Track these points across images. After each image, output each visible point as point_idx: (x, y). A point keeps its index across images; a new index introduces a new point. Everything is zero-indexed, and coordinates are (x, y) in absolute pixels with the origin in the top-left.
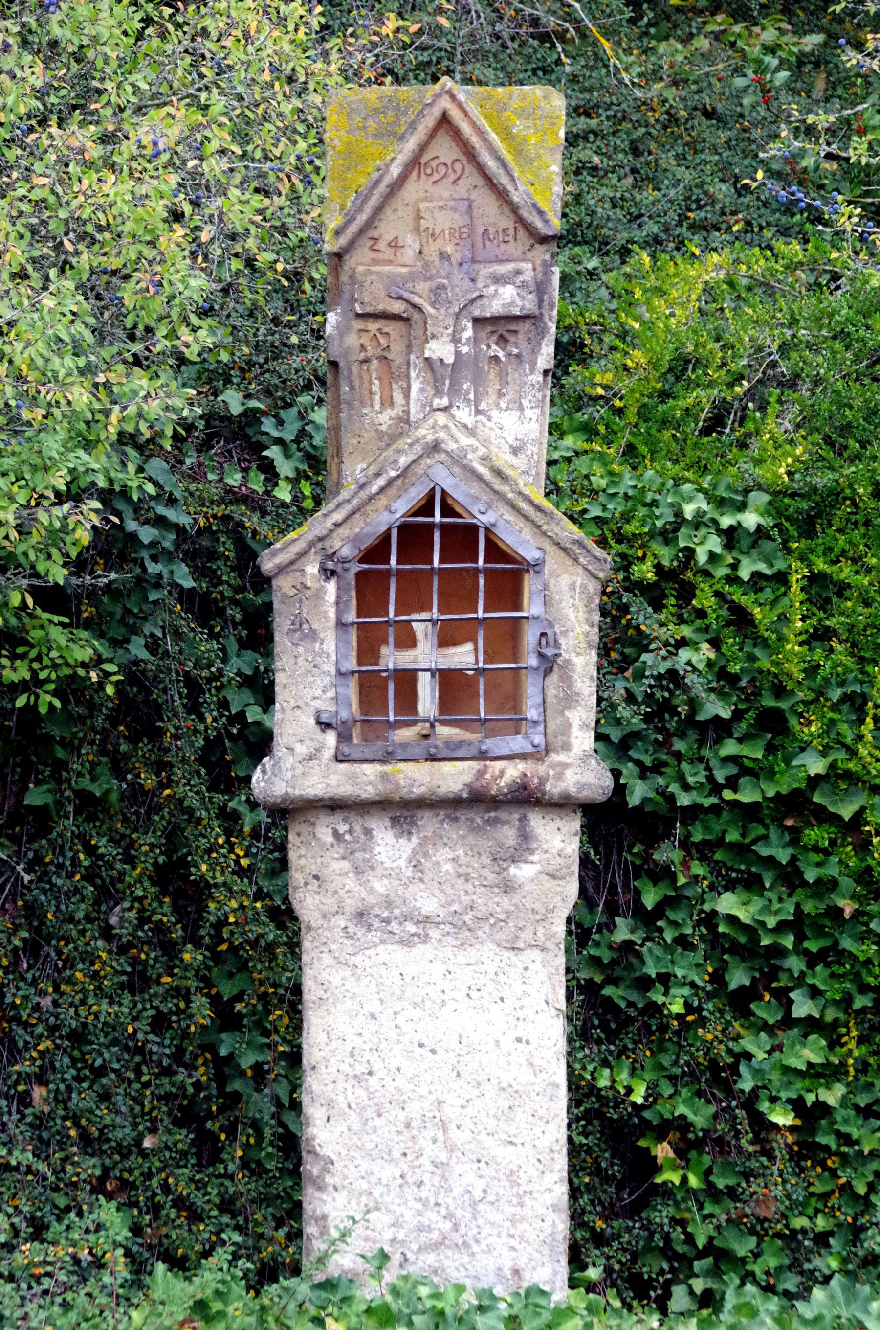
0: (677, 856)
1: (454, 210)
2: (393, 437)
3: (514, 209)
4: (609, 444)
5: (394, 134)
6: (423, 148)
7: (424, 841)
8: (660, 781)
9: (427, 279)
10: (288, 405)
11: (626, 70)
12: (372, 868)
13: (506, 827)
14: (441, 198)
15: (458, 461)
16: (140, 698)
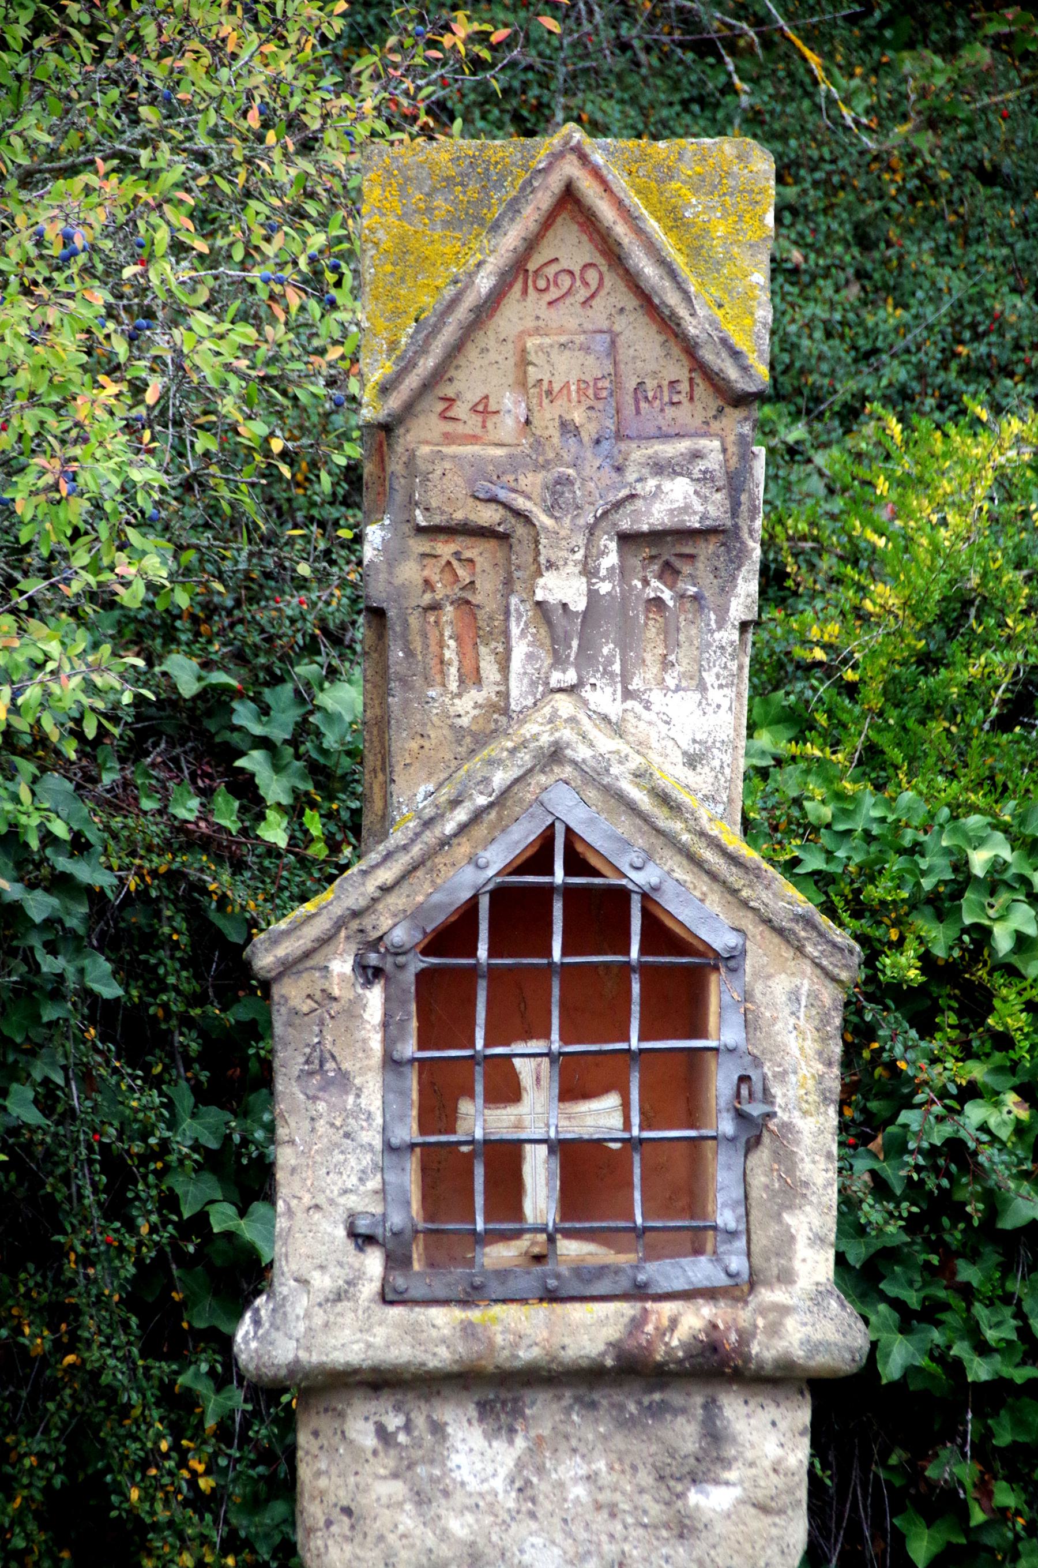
0: (967, 1472)
1: (586, 349)
2: (480, 739)
3: (690, 349)
4: (835, 745)
5: (481, 221)
6: (531, 244)
7: (538, 1444)
8: (937, 1336)
9: (538, 467)
10: (276, 681)
11: (847, 101)
12: (446, 1494)
13: (681, 1420)
14: (562, 330)
15: (594, 779)
16: (21, 1192)
